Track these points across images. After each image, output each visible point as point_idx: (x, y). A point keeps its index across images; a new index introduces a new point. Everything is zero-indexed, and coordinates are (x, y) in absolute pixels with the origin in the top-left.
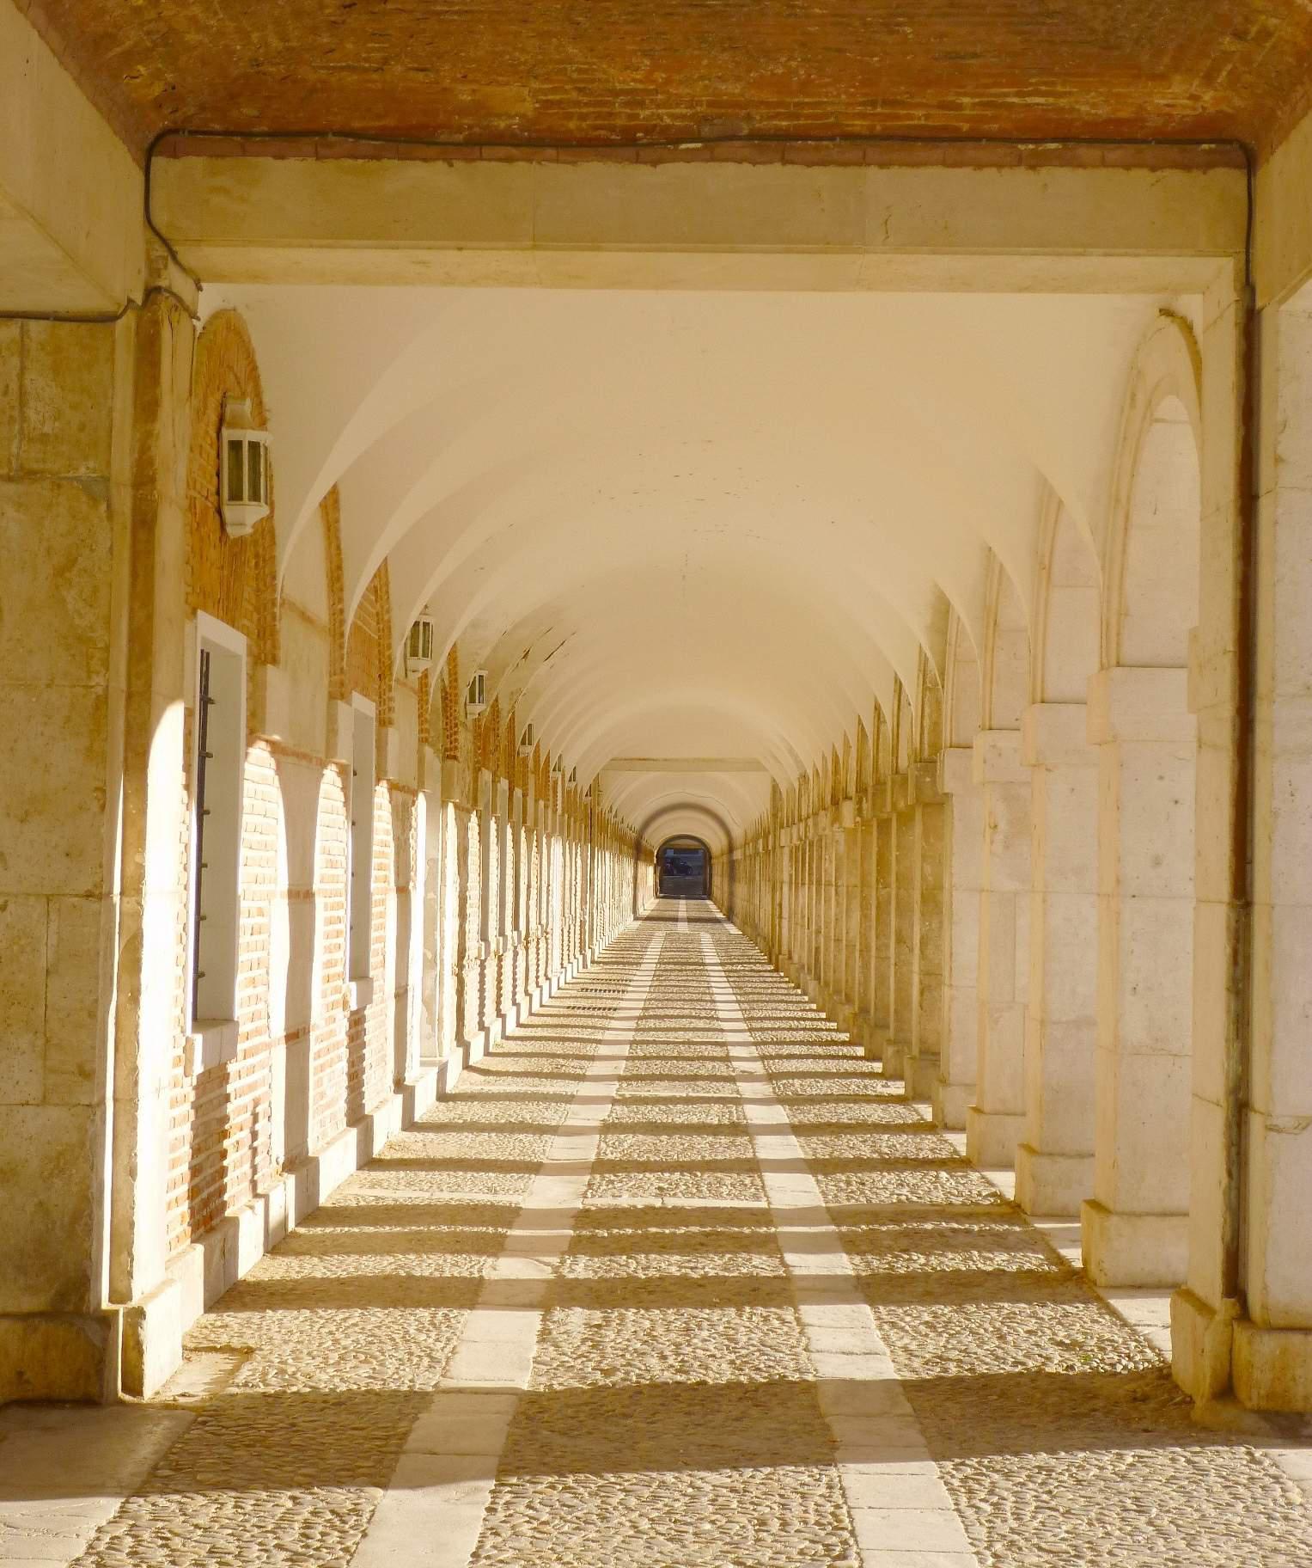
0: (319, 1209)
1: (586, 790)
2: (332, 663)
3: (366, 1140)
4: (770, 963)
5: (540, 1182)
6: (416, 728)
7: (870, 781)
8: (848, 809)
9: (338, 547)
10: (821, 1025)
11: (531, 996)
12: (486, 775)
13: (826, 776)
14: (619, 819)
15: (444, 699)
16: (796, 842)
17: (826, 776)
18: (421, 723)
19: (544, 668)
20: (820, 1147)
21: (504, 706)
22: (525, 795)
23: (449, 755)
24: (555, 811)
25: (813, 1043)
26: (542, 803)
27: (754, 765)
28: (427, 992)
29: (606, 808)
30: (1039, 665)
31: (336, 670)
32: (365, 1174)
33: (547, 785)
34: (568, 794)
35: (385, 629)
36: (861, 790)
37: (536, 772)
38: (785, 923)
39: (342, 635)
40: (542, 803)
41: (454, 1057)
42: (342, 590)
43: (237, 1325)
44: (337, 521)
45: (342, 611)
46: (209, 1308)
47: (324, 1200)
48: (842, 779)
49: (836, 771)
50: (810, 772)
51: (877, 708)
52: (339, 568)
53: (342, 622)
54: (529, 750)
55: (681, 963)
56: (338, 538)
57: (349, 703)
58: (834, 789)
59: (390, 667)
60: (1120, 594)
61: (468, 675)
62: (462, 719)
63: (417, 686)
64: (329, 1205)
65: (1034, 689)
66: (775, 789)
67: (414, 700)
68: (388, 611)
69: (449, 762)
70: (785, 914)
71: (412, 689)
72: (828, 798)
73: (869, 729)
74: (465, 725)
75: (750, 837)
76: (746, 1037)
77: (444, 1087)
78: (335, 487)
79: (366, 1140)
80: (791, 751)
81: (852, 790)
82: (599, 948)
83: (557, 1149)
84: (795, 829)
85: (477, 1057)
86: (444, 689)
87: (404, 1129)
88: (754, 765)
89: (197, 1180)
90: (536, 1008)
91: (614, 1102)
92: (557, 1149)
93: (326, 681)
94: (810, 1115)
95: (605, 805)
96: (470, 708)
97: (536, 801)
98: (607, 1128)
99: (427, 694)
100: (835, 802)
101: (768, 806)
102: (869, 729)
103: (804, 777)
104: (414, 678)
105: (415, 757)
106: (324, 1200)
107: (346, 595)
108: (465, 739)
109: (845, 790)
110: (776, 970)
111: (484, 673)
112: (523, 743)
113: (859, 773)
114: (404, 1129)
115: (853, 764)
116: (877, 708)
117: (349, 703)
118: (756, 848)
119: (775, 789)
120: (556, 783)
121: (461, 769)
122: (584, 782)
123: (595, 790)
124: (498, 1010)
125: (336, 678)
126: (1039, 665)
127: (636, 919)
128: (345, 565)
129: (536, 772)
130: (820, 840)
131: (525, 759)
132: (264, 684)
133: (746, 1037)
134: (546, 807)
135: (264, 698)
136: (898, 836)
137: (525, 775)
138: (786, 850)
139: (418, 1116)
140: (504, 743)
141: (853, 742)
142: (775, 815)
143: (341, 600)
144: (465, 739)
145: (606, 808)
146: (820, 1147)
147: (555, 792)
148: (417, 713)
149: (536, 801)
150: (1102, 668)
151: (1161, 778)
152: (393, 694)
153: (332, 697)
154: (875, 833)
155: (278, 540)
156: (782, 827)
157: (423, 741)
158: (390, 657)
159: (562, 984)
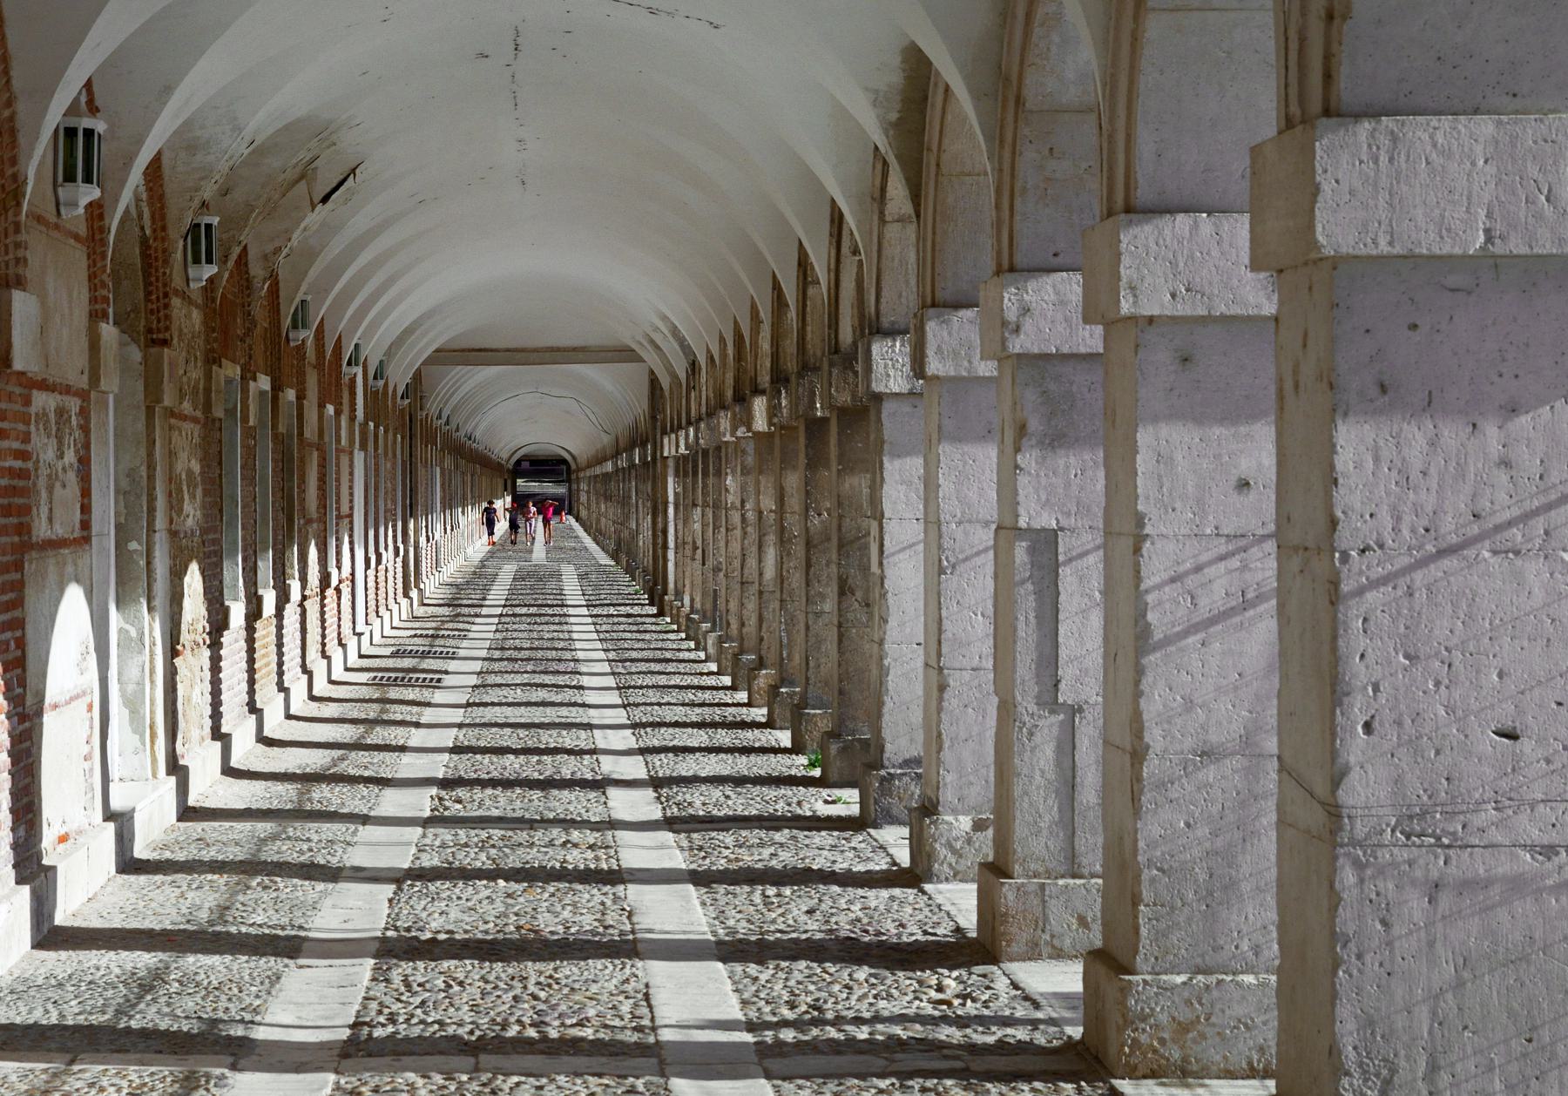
1: (401, 390)
4: (651, 604)
7: (791, 365)
11: (328, 658)
13: (724, 364)
15: (145, 255)
17: (724, 364)
19: (315, 218)
21: (257, 270)
22: (301, 397)
24: (352, 418)
25: (714, 725)
26: (330, 409)
27: (624, 354)
28: (131, 688)
30: (1121, 157)
33: (339, 384)
34: (373, 397)
36: (780, 379)
37: (319, 365)
38: (671, 555)
40: (330, 409)
41: (202, 758)
47: (60, 919)
48: (750, 367)
49: (739, 357)
50: (702, 360)
54: (307, 335)
55: (536, 597)
58: (737, 380)
61: (181, 217)
62: (177, 282)
63: (82, 230)
65: (999, 253)
66: (654, 382)
70: (671, 544)
72: (729, 393)
73: (791, 295)
74: (184, 296)
75: (622, 445)
77: (186, 800)
80: (675, 331)
81: (765, 380)
83: (392, 802)
84: (682, 433)
85: (321, 687)
86: (144, 242)
87: (38, 944)
90: (353, 660)
95: (432, 407)
97: (321, 406)
99: (103, 242)
101: (645, 405)
102: (791, 295)
103: (693, 366)
105: (84, 342)
108: (188, 319)
109: (754, 381)
110: (661, 614)
111: (215, 221)
113: (776, 357)
114: (38, 944)
115: (765, 345)
116: (754, 307)
118: (631, 459)
119: (654, 382)
120: (353, 381)
121: (181, 364)
122: (399, 377)
123: (416, 387)
124: (340, 640)
130: (718, 448)
131: (302, 347)
133: (620, 716)
134: (338, 413)
136: (840, 444)
137: (301, 376)
138: (671, 463)
139: (316, 692)
140: (263, 323)
141: (765, 314)
142: (653, 418)
144: (188, 319)
147: (353, 394)
148: (84, 275)
149: (321, 406)
151: (1414, 327)
152: (23, 237)
154: (802, 440)
156: (664, 432)
158: (15, 177)
159: (156, 825)
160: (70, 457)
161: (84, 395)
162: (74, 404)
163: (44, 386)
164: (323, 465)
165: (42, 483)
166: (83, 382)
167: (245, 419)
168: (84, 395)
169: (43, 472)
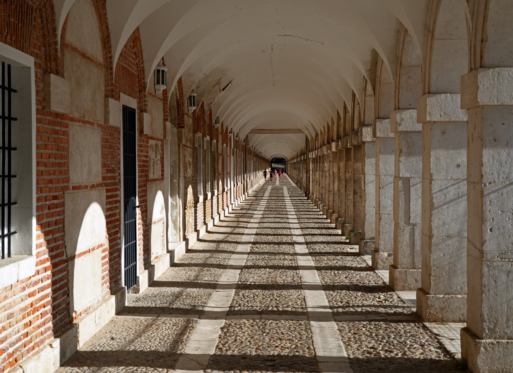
0: (77, 352)
2: (106, 81)
3: (172, 258)
4: (306, 196)
5: (244, 237)
6: (162, 114)
7: (342, 134)
8: (334, 144)
9: (107, 27)
10: (349, 261)
12: (200, 135)
14: (256, 150)
15: (178, 104)
16: (314, 156)
18: (164, 112)
20: (329, 277)
22: (217, 142)
23: (180, 126)
24: (230, 147)
25: (322, 228)
26: (225, 145)
27: (300, 131)
28: (174, 218)
29: (251, 146)
30: (427, 79)
31: (108, 82)
32: (149, 288)
34: (236, 142)
35: (142, 71)
36: (339, 138)
38: (311, 184)
39: (112, 68)
40: (225, 145)
42: (110, 47)
43: (190, 255)
44: (105, 14)
45: (111, 58)
46: (61, 366)
47: (156, 279)
48: (331, 135)
49: (328, 132)
50: (319, 132)
51: (345, 107)
52: (108, 37)
53: (111, 63)
54: (219, 125)
55: (277, 195)
56: (106, 23)
57: (118, 99)
58: (328, 138)
59: (145, 87)
60: (483, 31)
61: (187, 94)
62: (186, 111)
63: (162, 97)
64: (157, 280)
66: (307, 139)
67: (161, 104)
68: (142, 63)
69: (180, 129)
70: (311, 181)
71: (160, 99)
72: (326, 141)
73: (342, 116)
74: (187, 115)
76: (298, 226)
78: (138, 29)
79: (172, 258)
80: (312, 125)
81: (335, 138)
82: (250, 191)
83: (240, 248)
84: (314, 152)
88: (300, 131)
89: (54, 312)
90: (230, 211)
91: (257, 228)
92: (245, 238)
93: (103, 88)
94: (325, 261)
96: (190, 108)
97: (223, 144)
98: (257, 234)
99: (167, 100)
100: (329, 143)
102: (342, 116)
103: (317, 134)
104: (160, 93)
105: (162, 127)
106: (156, 279)
107: (113, 50)
108: (189, 121)
110: (308, 199)
111: (195, 95)
112: (216, 123)
115: (335, 129)
117: (118, 99)
119: (307, 139)
120: (231, 138)
122: (242, 137)
123: (246, 139)
125: (109, 88)
126: (427, 79)
127: (214, 226)
128: (111, 36)
129: (222, 134)
130: (323, 156)
132: (49, 83)
134: (227, 146)
135: (49, 91)
138: (311, 160)
141: (335, 121)
143: (110, 52)
144: (189, 121)
145: (251, 146)
146: (329, 277)
147: (231, 141)
148: (162, 109)
149: (223, 144)
150: (471, 70)
152: (146, 99)
153: (106, 96)
155: (56, 9)
156: (309, 152)
157: (165, 120)
158: (144, 83)
160: (159, 157)
161: (162, 141)
162: (160, 143)
163: (152, 138)
164: (223, 160)
165: (151, 164)
166: (162, 137)
167: (203, 147)
168: (162, 141)
169: (152, 161)
